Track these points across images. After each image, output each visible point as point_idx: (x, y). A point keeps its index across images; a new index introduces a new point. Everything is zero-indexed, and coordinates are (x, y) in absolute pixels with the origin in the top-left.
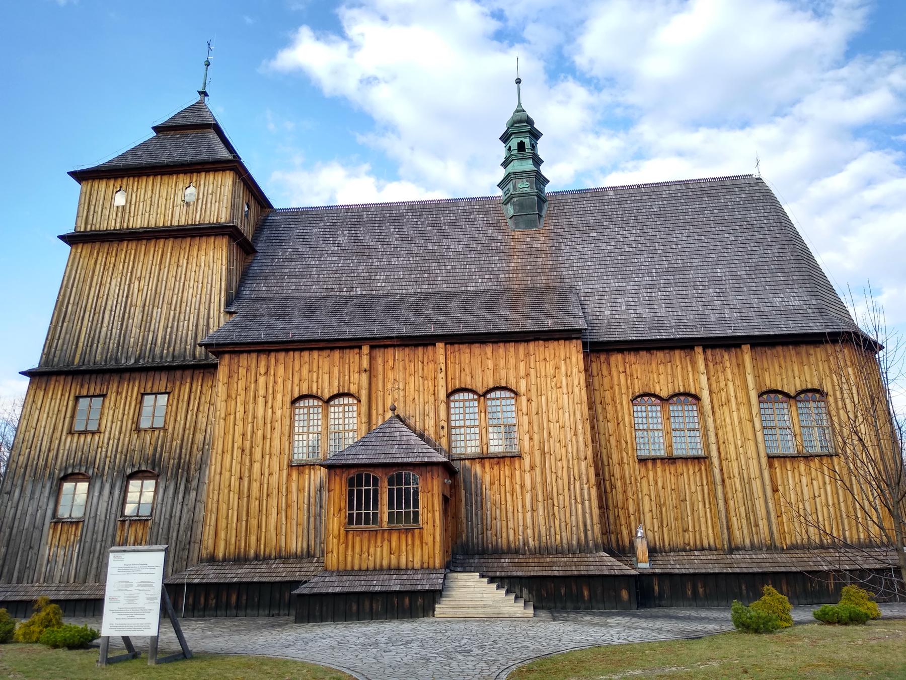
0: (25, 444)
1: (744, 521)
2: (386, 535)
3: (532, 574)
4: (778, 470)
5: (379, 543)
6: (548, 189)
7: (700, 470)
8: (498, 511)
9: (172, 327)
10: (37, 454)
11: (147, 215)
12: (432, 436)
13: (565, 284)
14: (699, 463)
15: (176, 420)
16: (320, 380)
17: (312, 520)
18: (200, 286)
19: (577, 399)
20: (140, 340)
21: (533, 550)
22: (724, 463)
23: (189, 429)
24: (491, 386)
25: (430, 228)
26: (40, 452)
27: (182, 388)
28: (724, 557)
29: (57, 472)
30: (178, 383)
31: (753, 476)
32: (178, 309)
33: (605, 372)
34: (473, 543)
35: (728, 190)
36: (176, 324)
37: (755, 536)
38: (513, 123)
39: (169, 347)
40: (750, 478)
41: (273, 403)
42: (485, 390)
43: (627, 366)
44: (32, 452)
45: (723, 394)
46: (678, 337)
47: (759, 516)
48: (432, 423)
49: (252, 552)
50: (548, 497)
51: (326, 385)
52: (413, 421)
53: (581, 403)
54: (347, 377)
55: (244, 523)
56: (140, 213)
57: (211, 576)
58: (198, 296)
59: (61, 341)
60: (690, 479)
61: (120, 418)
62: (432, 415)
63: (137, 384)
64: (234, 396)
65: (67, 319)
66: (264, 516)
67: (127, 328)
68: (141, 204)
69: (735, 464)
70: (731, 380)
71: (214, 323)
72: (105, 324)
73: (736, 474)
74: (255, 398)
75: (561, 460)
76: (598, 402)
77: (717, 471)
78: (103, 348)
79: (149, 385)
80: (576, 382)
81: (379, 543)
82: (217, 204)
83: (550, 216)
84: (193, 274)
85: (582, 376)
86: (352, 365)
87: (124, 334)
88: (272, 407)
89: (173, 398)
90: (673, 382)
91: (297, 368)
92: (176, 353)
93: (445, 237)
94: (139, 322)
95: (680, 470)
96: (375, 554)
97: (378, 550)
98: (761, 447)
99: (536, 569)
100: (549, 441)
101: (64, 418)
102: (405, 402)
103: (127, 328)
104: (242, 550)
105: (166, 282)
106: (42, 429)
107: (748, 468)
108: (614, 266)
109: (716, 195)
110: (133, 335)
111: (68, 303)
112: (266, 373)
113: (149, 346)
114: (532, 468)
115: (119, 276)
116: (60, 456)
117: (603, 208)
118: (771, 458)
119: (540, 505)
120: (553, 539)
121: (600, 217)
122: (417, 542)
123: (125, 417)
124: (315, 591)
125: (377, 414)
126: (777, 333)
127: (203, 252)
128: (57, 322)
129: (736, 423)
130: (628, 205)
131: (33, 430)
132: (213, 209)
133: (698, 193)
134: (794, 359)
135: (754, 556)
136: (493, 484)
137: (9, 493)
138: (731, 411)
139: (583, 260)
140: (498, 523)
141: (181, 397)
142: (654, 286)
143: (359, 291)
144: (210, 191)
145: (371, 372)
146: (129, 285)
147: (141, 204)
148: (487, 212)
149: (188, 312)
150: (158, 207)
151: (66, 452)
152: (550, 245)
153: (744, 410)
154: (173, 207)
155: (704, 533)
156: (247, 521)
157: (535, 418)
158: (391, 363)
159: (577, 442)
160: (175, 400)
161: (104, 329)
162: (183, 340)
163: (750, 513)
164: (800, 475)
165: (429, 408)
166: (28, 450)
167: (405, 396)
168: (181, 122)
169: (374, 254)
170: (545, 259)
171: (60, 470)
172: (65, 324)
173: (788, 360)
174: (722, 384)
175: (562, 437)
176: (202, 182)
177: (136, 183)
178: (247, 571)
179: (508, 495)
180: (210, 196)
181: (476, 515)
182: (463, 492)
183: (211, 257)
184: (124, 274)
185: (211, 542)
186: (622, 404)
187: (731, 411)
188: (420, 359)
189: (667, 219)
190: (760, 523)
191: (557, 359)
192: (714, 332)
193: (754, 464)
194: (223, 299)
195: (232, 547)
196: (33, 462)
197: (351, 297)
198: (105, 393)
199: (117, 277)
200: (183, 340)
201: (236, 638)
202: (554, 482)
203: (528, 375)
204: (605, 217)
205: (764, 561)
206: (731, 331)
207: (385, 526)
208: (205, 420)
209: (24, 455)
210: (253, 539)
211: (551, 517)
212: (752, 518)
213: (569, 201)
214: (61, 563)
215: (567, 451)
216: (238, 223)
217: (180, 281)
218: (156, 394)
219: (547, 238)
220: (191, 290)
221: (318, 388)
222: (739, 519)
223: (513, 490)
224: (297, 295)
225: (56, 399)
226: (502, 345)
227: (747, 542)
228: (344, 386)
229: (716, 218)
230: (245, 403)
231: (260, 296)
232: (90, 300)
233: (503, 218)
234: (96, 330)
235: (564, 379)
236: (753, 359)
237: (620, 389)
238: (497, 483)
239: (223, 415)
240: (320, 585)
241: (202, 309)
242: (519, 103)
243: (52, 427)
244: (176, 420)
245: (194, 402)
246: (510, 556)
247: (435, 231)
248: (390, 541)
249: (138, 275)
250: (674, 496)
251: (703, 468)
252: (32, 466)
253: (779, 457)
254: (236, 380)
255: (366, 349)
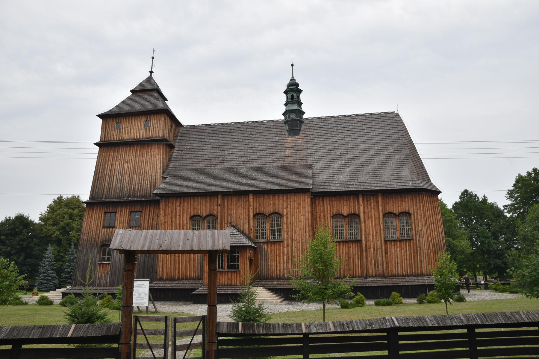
0: (86, 232)
1: (373, 266)
2: (226, 273)
3: (285, 287)
4: (388, 245)
5: (224, 276)
6: (305, 116)
7: (358, 246)
8: (273, 263)
9: (141, 183)
10: (91, 236)
11: (129, 133)
12: (247, 232)
13: (308, 164)
14: (357, 243)
15: (144, 223)
16: (201, 209)
17: (199, 265)
18: (152, 165)
19: (307, 218)
20: (129, 189)
21: (286, 278)
22: (368, 242)
23: (150, 227)
24: (272, 212)
25: (251, 135)
26: (92, 235)
27: (146, 209)
28: (364, 280)
29: (99, 243)
30: (144, 208)
31: (378, 248)
32: (143, 175)
33: (321, 205)
34: (263, 275)
35: (383, 119)
36: (142, 182)
37: (377, 272)
38: (289, 85)
39: (140, 192)
40: (377, 249)
41: (182, 218)
42: (269, 213)
43: (331, 202)
44: (89, 235)
45: (370, 214)
46: (352, 190)
47: (380, 264)
48: (247, 227)
49: (176, 277)
50: (293, 257)
51: (204, 211)
52: (239, 226)
53: (308, 220)
54: (212, 208)
55: (173, 266)
56: (126, 133)
57: (161, 286)
58: (151, 170)
59: (97, 189)
60: (354, 249)
61: (122, 222)
62: (247, 224)
63: (128, 208)
64: (167, 215)
65: (99, 180)
66: (181, 264)
67: (123, 183)
68: (127, 129)
69: (372, 243)
70: (373, 208)
71: (158, 181)
72: (114, 182)
73: (372, 247)
74: (175, 216)
75: (299, 243)
76: (318, 217)
77: (364, 246)
78: (114, 192)
79: (133, 208)
80: (307, 210)
81: (224, 276)
82: (158, 128)
83: (305, 130)
84: (149, 160)
85: (309, 208)
86: (214, 202)
87: (123, 187)
88: (182, 220)
89: (143, 214)
90: (349, 209)
91: (192, 203)
92: (143, 194)
93: (257, 140)
94: (128, 181)
95: (349, 246)
96: (222, 280)
97: (224, 278)
98: (382, 236)
99: (286, 285)
100: (295, 235)
101: (101, 221)
102: (236, 218)
103: (123, 183)
104: (173, 276)
105: (138, 164)
106: (92, 226)
107: (377, 245)
108: (330, 155)
109: (378, 121)
110: (126, 187)
111: (99, 172)
112: (179, 206)
113: (132, 191)
114: (288, 246)
115: (119, 161)
116: (100, 236)
117: (328, 126)
118: (386, 241)
119: (290, 261)
120: (294, 274)
121: (326, 131)
122: (238, 276)
123: (124, 221)
124: (200, 293)
125: (225, 223)
126: (392, 188)
127: (153, 150)
128: (95, 181)
129: (374, 226)
130: (340, 125)
131: (89, 226)
132: (156, 131)
133: (371, 120)
134: (399, 199)
135: (375, 280)
136: (271, 252)
137: (81, 251)
138: (372, 221)
139: (317, 152)
140: (273, 268)
141: (146, 213)
142: (346, 165)
143: (219, 166)
144: (155, 123)
145: (222, 206)
146: (123, 165)
147: (127, 129)
148: (277, 128)
149: (147, 177)
150: (134, 130)
151: (102, 235)
152: (303, 144)
153: (377, 221)
154: (140, 130)
155: (357, 271)
156: (174, 265)
157: (289, 225)
158: (230, 202)
159: (306, 235)
160: (144, 215)
161: (114, 184)
162: (146, 189)
163: (376, 262)
164: (397, 247)
165: (246, 221)
166: (87, 234)
167: (236, 216)
168: (142, 88)
169: (226, 148)
170: (300, 151)
171: (101, 243)
172: (99, 182)
173: (397, 200)
174: (369, 210)
175: (300, 233)
176: (152, 118)
177: (124, 120)
178: (175, 284)
179: (277, 257)
180: (155, 125)
181: (265, 264)
182: (259, 255)
183: (156, 152)
184: (121, 160)
185: (161, 273)
186: (328, 218)
187: (372, 221)
188: (243, 200)
189: (356, 132)
190: (380, 266)
191: (299, 200)
192: (367, 188)
193: (379, 243)
194: (161, 171)
195: (169, 275)
196: (90, 239)
197: (215, 169)
198: (116, 211)
199: (118, 161)
200: (146, 189)
201: (172, 308)
202: (296, 251)
203: (287, 207)
204: (328, 131)
205: (379, 281)
206: (374, 187)
207: (226, 270)
208: (156, 223)
209: (86, 236)
210: (177, 272)
211: (294, 265)
212: (376, 264)
213: (314, 122)
214: (103, 279)
215: (302, 239)
216: (167, 136)
217: (143, 163)
218: (136, 212)
219: (303, 141)
220: (148, 167)
221: (200, 212)
222: (372, 265)
223: (279, 255)
224: (192, 168)
225: (97, 213)
226: (277, 195)
227: (374, 274)
228: (211, 212)
229: (377, 133)
230: (172, 218)
231: (177, 168)
232: (108, 171)
233: (284, 130)
234: (111, 184)
235: (302, 209)
236: (382, 199)
237: (327, 212)
238: (273, 252)
239: (163, 223)
240: (202, 291)
241: (153, 175)
242: (293, 77)
243: (96, 225)
244: (144, 223)
245: (151, 216)
246: (277, 280)
247: (253, 137)
248: (228, 275)
249: (127, 160)
250: (346, 256)
251: (359, 245)
252: (89, 241)
253: (389, 240)
254: (168, 208)
255: (220, 196)
